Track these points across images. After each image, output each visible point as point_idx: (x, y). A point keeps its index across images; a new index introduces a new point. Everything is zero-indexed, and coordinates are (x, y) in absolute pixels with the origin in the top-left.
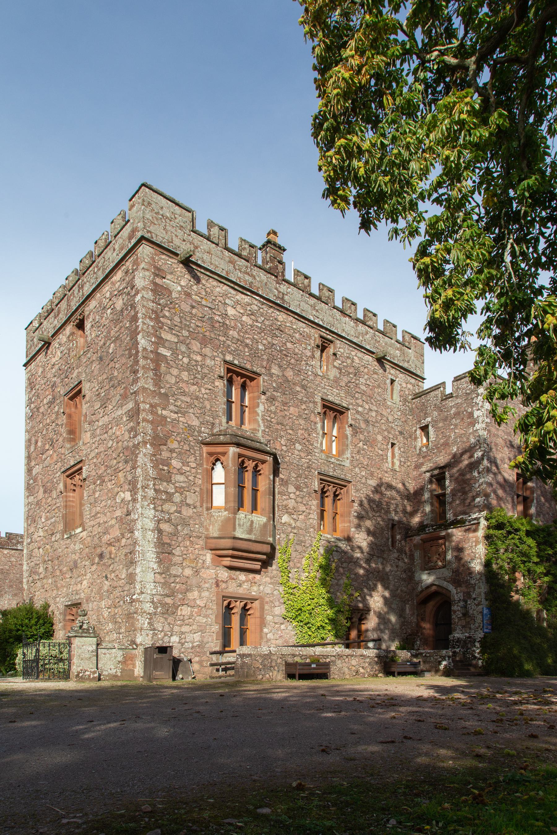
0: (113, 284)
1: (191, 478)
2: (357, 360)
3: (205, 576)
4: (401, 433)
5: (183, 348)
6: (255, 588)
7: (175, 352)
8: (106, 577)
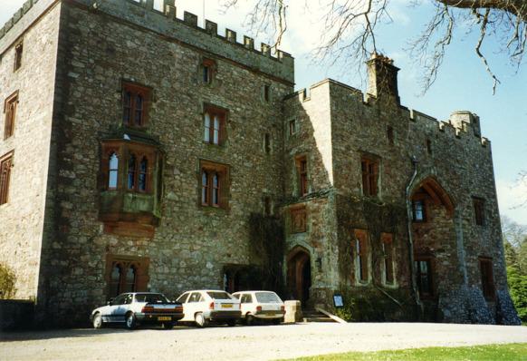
0: (41, 25)
1: (90, 167)
2: (235, 73)
3: (98, 243)
4: (274, 126)
5: (89, 72)
6: (141, 252)
7: (82, 75)
8: (20, 244)
